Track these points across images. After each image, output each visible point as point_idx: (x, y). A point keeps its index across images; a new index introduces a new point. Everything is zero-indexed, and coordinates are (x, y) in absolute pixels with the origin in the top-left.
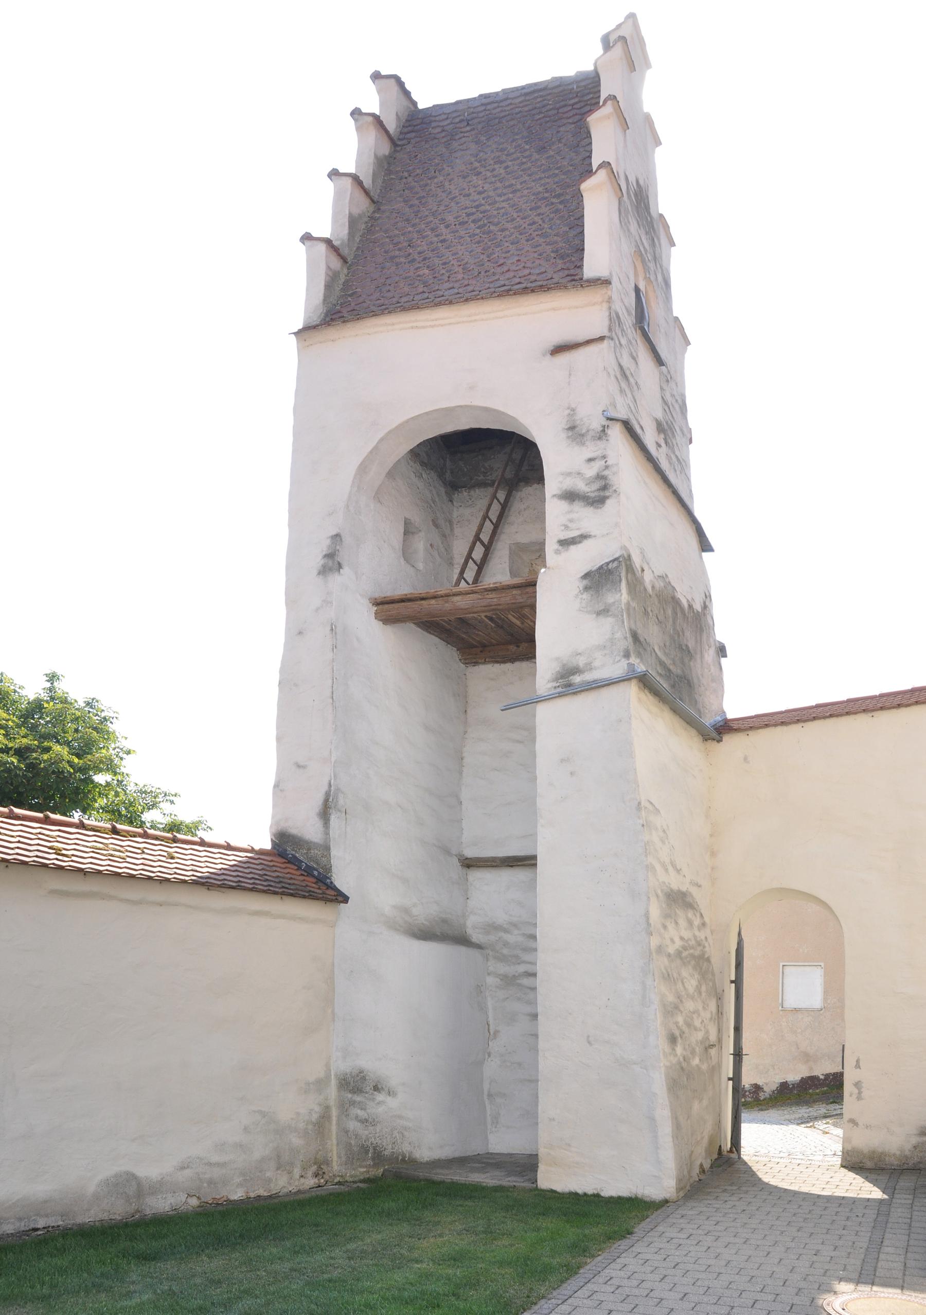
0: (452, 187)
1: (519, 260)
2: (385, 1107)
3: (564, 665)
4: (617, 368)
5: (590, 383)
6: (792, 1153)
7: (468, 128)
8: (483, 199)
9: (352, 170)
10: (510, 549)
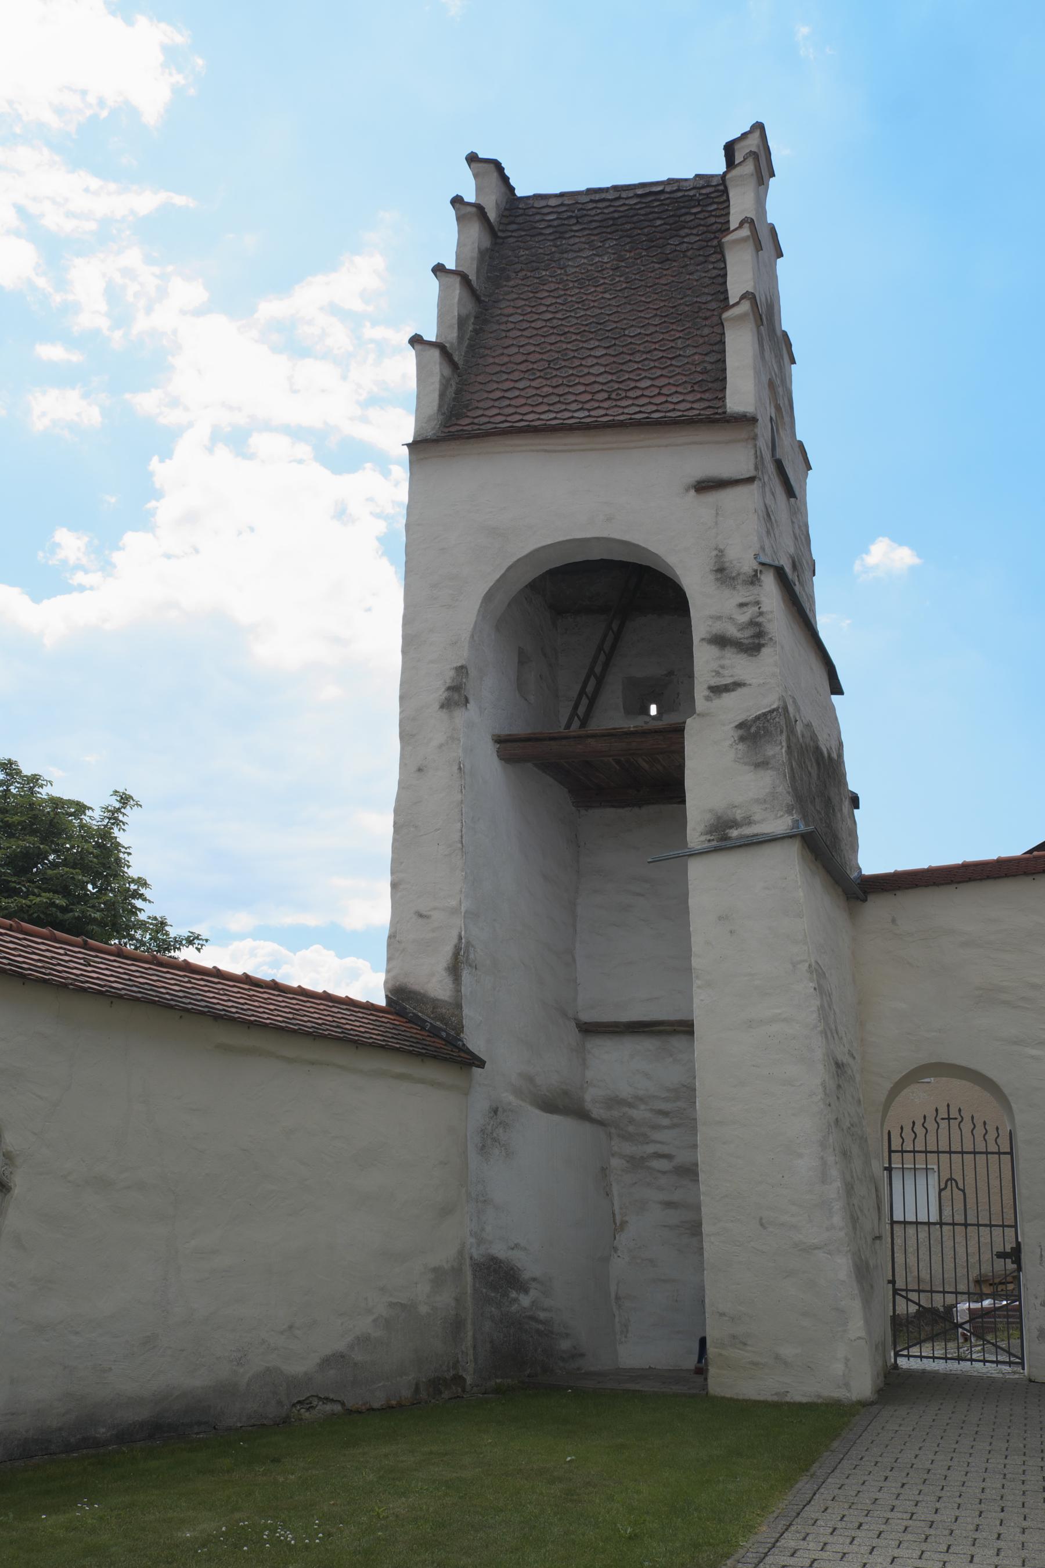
3: (719, 818)
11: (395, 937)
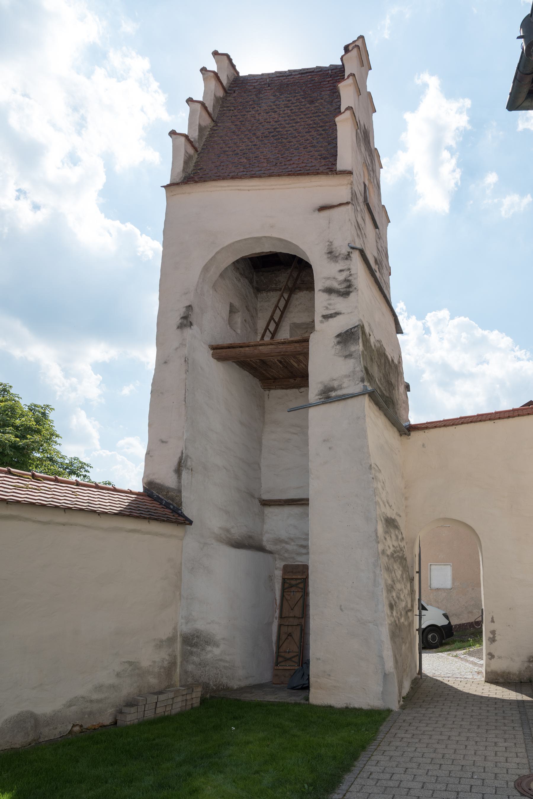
0: (260, 118)
1: (299, 159)
2: (214, 653)
3: (325, 386)
4: (355, 221)
5: (342, 229)
6: (455, 669)
7: (269, 88)
8: (278, 125)
9: (201, 99)
10: (290, 326)
11: (149, 454)
